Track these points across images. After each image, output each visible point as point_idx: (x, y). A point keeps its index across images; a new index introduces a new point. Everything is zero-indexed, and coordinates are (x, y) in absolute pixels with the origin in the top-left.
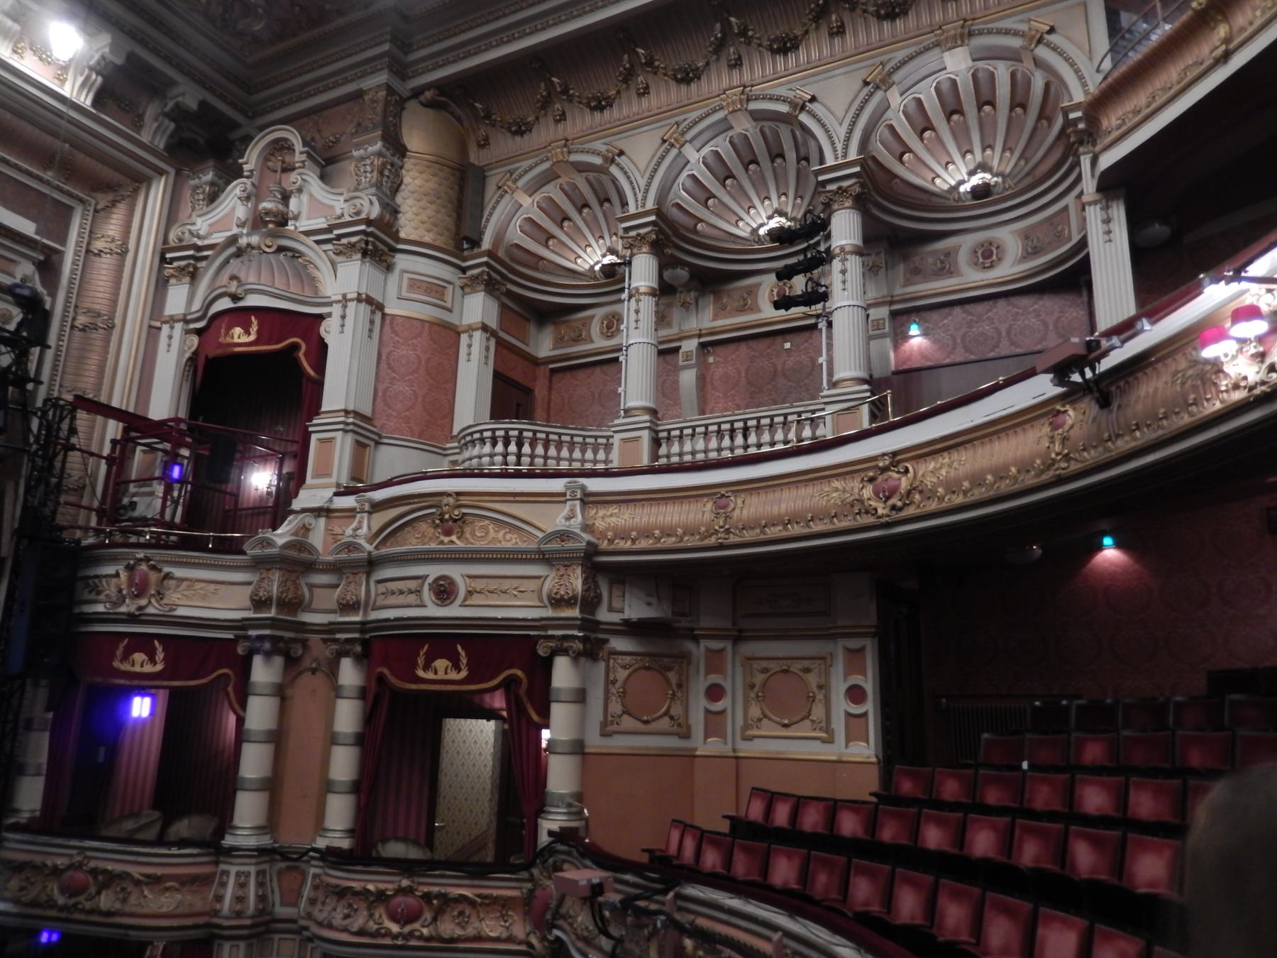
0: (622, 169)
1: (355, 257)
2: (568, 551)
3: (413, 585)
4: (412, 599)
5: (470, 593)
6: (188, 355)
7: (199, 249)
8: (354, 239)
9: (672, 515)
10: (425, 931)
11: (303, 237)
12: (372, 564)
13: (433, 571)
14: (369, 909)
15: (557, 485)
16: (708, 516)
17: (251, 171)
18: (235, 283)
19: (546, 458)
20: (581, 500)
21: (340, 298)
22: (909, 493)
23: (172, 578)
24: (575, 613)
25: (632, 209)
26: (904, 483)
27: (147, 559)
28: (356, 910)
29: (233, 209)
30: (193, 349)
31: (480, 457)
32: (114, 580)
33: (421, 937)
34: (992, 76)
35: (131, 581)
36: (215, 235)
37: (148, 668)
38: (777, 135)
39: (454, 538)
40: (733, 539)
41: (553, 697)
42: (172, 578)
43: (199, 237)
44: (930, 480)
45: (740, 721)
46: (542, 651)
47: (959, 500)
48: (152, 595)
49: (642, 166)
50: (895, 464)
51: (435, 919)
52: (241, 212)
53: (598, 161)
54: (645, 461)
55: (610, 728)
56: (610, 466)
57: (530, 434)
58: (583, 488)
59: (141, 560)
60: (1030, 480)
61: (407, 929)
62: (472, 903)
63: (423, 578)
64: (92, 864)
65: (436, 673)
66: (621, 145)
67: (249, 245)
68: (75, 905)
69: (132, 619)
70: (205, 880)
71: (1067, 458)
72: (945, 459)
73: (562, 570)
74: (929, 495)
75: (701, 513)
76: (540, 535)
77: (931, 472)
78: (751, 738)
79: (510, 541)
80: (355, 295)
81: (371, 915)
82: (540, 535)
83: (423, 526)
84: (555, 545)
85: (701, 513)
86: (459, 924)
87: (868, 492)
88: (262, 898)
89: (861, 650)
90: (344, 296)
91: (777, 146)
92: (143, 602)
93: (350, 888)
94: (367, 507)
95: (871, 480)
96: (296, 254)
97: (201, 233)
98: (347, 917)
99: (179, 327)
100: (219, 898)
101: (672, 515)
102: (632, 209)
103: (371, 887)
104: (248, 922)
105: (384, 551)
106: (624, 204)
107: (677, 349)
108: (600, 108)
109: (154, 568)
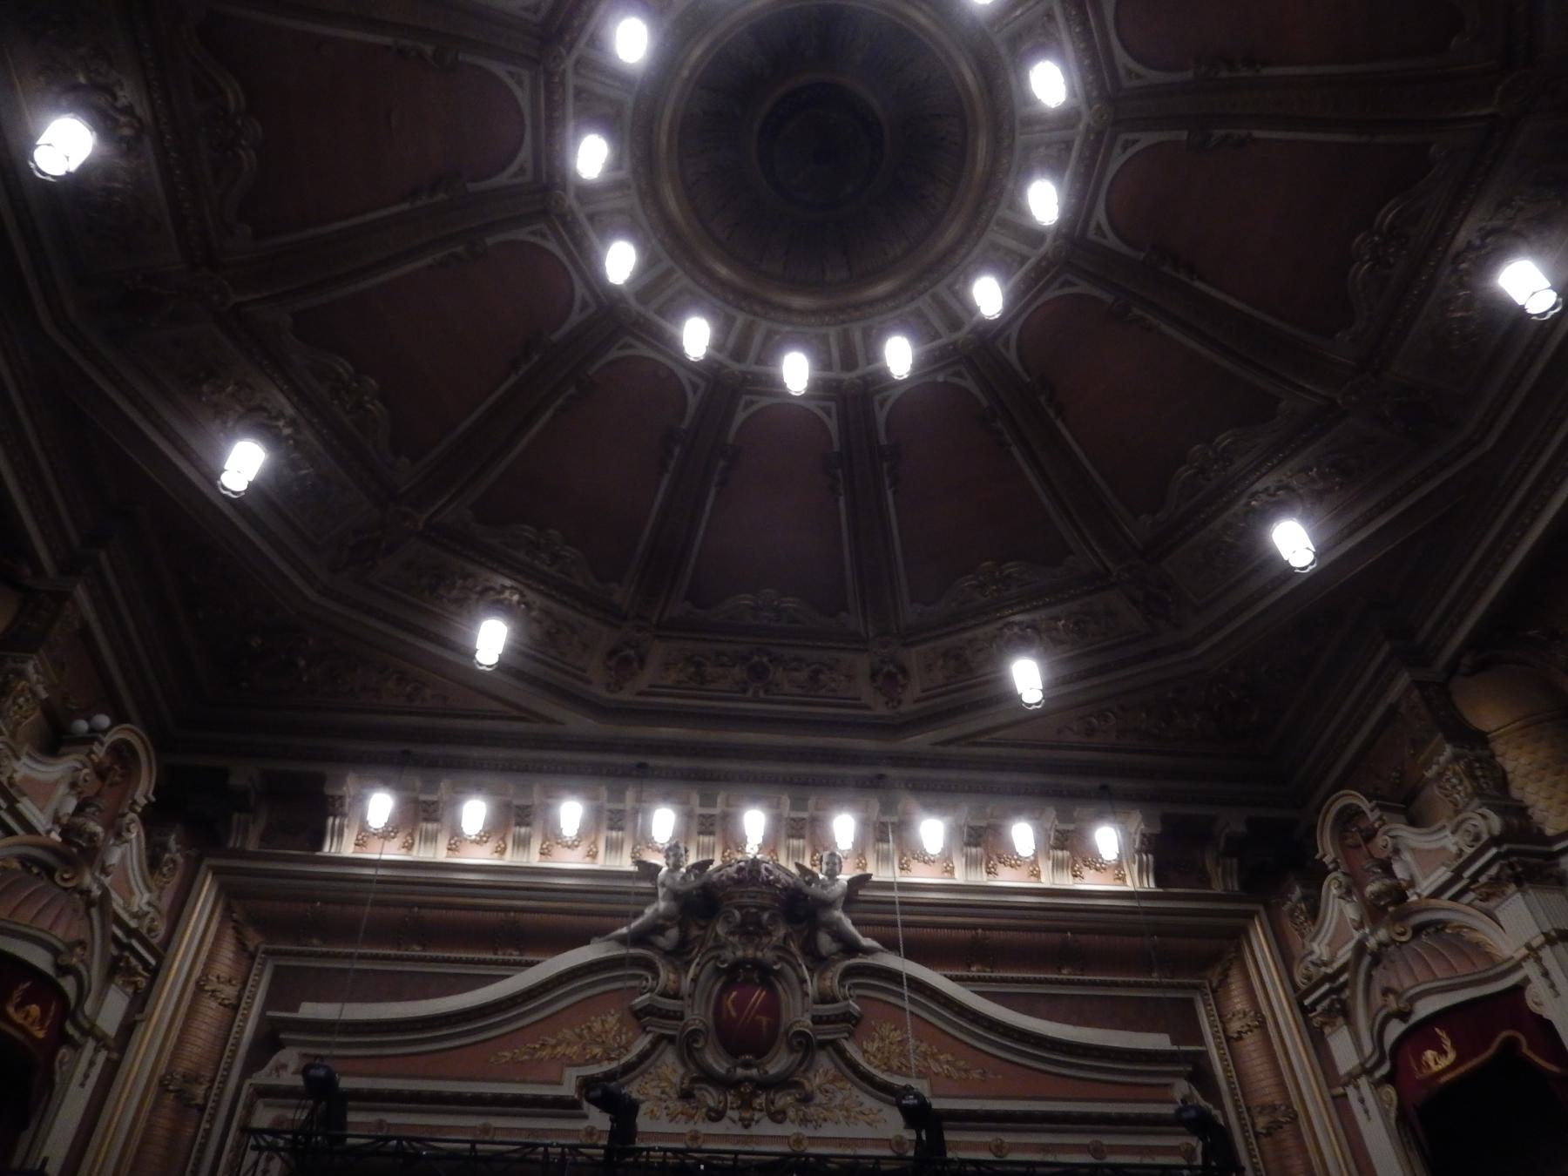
6: (1393, 1115)
7: (1332, 978)
8: (1493, 871)
36: (1340, 953)
43: (1325, 964)
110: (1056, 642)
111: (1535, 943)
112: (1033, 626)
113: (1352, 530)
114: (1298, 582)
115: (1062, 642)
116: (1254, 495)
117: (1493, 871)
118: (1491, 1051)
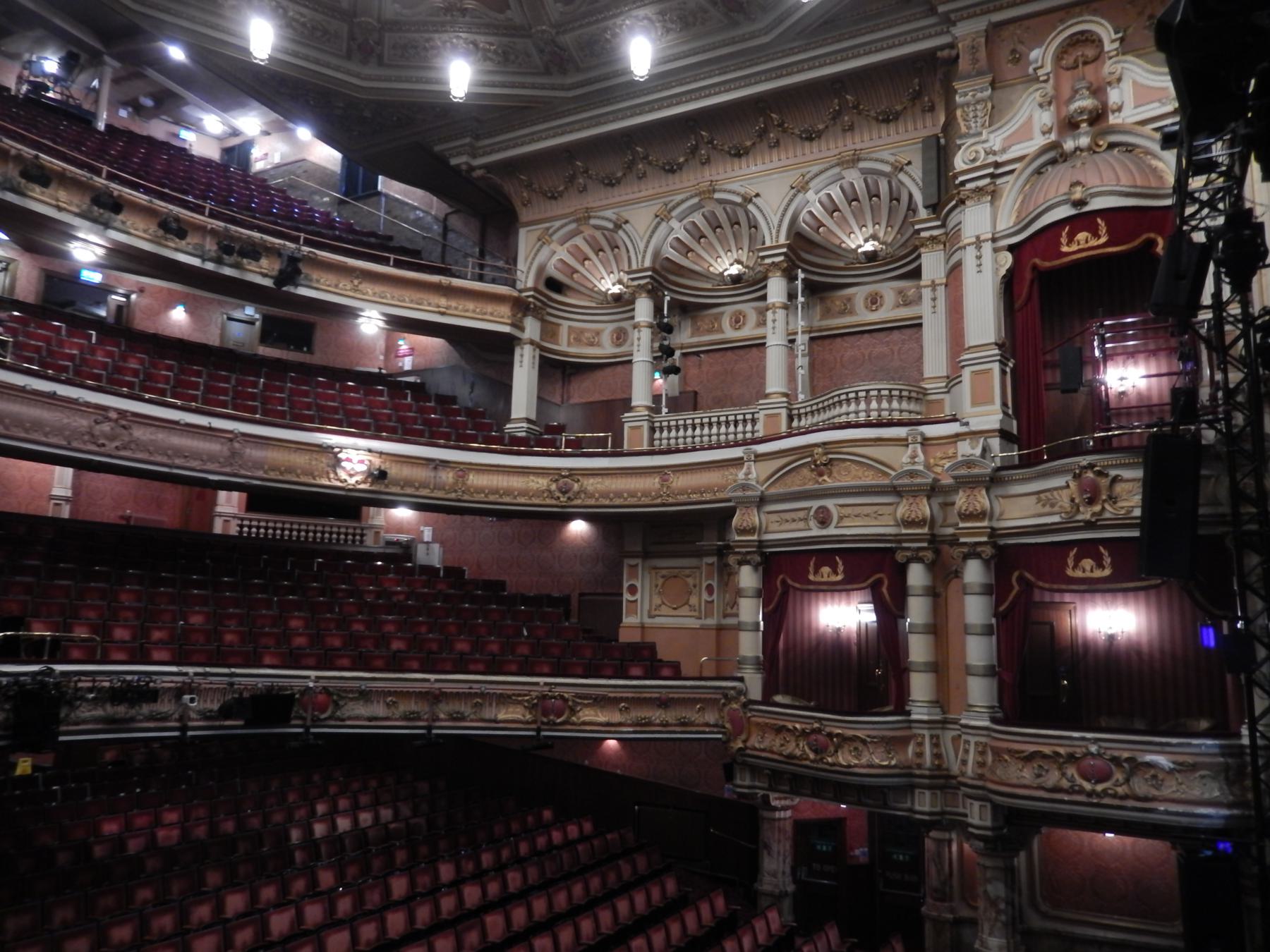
0: (758, 207)
1: (984, 199)
2: (972, 476)
3: (801, 514)
4: (801, 525)
5: (841, 518)
6: (1003, 272)
7: (997, 165)
8: (981, 183)
9: (516, 482)
10: (1120, 790)
11: (1139, 129)
12: (762, 501)
13: (815, 504)
14: (1060, 769)
15: (901, 432)
16: (657, 486)
17: (1048, 74)
18: (1079, 189)
19: (735, 434)
20: (922, 444)
21: (974, 240)
23: (1123, 480)
24: (926, 530)
27: (1091, 466)
28: (1047, 771)
29: (1031, 117)
30: (1008, 266)
31: (848, 414)
32: (1065, 491)
33: (1115, 796)
34: (577, 246)
35: (1082, 491)
36: (1014, 148)
37: (1098, 574)
38: (735, 213)
39: (825, 477)
41: (911, 592)
42: (1123, 480)
43: (995, 153)
45: (646, 607)
46: (900, 557)
48: (1104, 501)
51: (1127, 781)
52: (1046, 118)
54: (645, 447)
55: (654, 613)
56: (756, 435)
57: (886, 392)
58: (922, 434)
59: (1085, 467)
61: (1099, 788)
62: (864, 742)
63: (809, 509)
64: (828, 729)
65: (1084, 571)
67: (1077, 149)
68: (1104, 791)
69: (1089, 525)
70: (905, 741)
72: (599, 479)
73: (911, 500)
75: (653, 483)
76: (893, 473)
77: (591, 484)
78: (653, 617)
79: (869, 479)
80: (990, 236)
81: (1064, 775)
82: (893, 473)
83: (805, 471)
84: (906, 481)
85: (653, 483)
86: (1153, 786)
87: (554, 487)
88: (937, 756)
89: (637, 565)
90: (978, 238)
91: (735, 221)
92: (1097, 508)
93: (784, 726)
95: (556, 481)
96: (1129, 148)
97: (996, 148)
98: (782, 745)
99: (987, 248)
100: (920, 755)
101: (516, 482)
103: (1062, 751)
104: (927, 773)
105: (773, 491)
109: (1100, 474)
110: (486, 59)
111: (937, 282)
112: (475, 44)
113: (484, 85)
114: (806, 9)
115: (490, 59)
116: (458, 37)
117: (981, 183)
118: (1047, 264)
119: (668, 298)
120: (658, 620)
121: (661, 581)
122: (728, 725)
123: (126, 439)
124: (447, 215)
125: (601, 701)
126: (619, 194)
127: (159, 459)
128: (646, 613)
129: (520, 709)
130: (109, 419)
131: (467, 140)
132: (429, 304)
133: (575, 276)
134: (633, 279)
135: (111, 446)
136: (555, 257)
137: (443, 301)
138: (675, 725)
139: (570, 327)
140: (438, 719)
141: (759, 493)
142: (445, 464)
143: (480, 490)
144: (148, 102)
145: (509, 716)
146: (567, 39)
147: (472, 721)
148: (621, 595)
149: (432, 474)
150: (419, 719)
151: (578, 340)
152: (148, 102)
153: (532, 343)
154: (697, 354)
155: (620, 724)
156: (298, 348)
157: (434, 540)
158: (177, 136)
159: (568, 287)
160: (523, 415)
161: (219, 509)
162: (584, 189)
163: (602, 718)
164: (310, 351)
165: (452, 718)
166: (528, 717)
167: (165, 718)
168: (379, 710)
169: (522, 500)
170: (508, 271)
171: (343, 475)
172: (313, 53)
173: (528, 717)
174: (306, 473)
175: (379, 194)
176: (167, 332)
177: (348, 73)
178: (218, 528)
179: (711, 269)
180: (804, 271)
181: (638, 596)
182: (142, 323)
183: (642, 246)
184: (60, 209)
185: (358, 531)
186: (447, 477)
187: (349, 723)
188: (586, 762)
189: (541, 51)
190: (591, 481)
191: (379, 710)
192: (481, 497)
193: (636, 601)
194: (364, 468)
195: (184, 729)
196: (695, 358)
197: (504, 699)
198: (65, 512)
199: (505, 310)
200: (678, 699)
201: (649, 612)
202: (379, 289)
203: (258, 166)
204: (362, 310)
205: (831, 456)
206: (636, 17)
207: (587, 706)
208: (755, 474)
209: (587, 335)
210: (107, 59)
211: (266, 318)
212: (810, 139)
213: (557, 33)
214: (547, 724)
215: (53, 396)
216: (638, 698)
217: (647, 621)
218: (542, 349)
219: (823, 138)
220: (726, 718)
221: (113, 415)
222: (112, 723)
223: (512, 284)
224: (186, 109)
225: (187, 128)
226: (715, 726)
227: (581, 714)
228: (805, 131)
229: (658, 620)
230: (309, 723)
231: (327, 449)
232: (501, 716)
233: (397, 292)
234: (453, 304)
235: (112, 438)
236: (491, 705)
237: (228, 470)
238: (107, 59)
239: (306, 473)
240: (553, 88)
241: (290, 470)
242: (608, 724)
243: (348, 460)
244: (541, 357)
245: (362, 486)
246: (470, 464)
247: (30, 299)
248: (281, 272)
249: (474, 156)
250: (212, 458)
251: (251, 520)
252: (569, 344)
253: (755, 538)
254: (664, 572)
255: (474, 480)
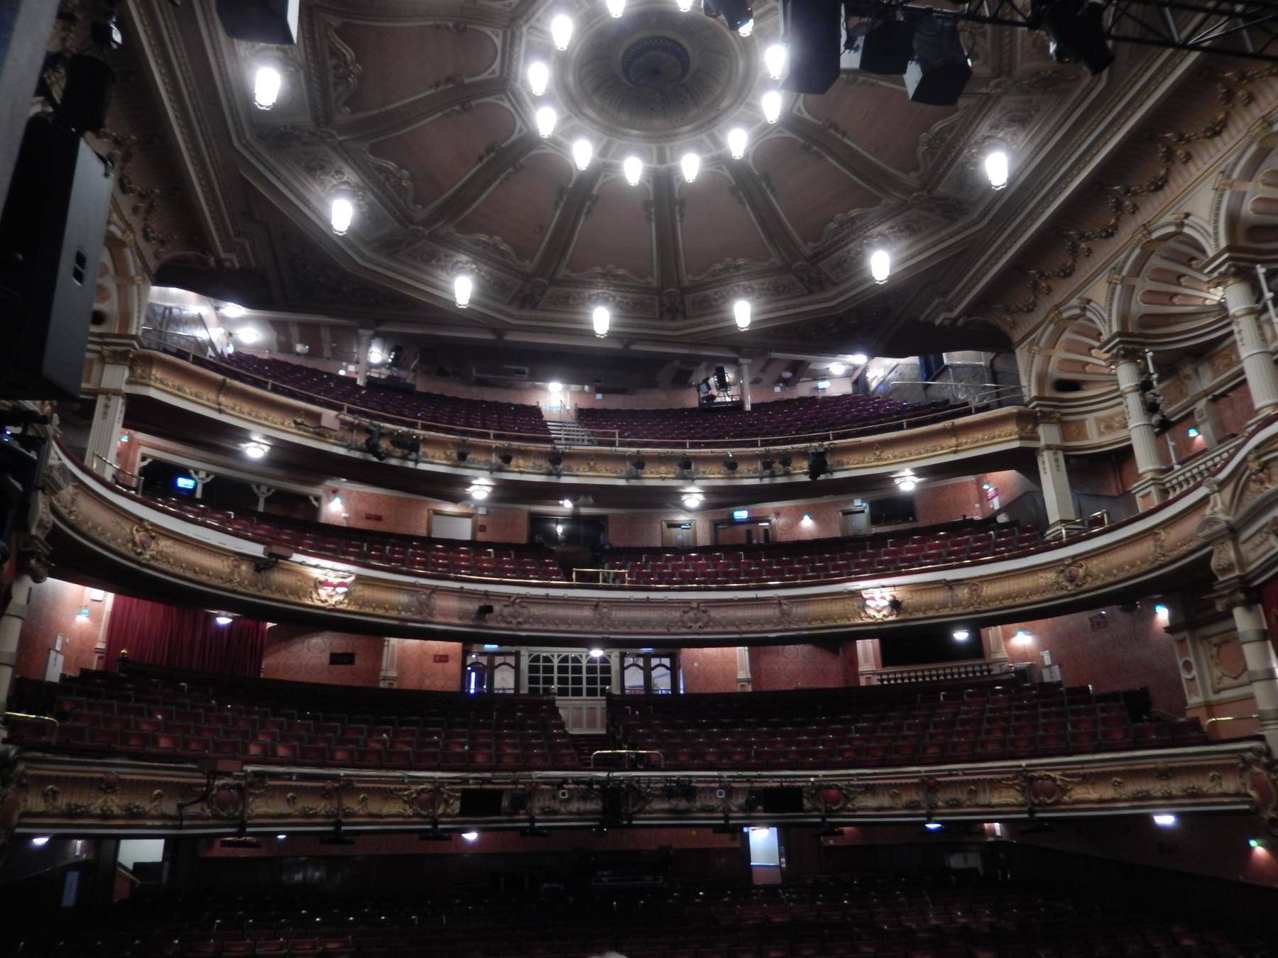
0: (1191, 227)
9: (1026, 583)
22: (1085, 577)
25: (1211, 253)
26: (1081, 571)
40: (983, 608)
44: (1095, 570)
45: (1208, 683)
47: (1111, 579)
49: (1206, 217)
50: (1074, 562)
53: (1172, 229)
60: (1146, 567)
66: (1186, 209)
71: (1164, 555)
72: (1102, 559)
74: (1097, 577)
75: (1146, 548)
77: (1095, 565)
85: (1147, 547)
94: (1216, 488)
101: (1026, 583)
102: (1211, 253)
106: (1203, 251)
107: (1191, 413)
108: (1110, 235)
119: (1150, 354)
120: (1226, 695)
121: (1215, 650)
122: (1253, 793)
123: (706, 619)
124: (992, 361)
125: (1088, 779)
126: (1077, 279)
127: (730, 629)
128: (1210, 691)
129: (1013, 792)
130: (692, 608)
131: (937, 301)
132: (943, 448)
133: (1087, 368)
134: (1107, 352)
135: (696, 627)
136: (1058, 361)
137: (953, 441)
138: (1182, 797)
139: (1099, 421)
140: (937, 807)
141: (1223, 525)
142: (959, 582)
143: (994, 598)
144: (788, 375)
145: (1002, 800)
146: (942, 190)
147: (968, 807)
148: (1179, 676)
149: (949, 594)
150: (921, 808)
151: (1109, 427)
152: (788, 375)
153: (1049, 447)
154: (1224, 395)
155: (1113, 800)
156: (905, 520)
157: (1054, 663)
158: (817, 388)
159: (1085, 382)
160: (1057, 518)
161: (861, 669)
162: (1049, 290)
163: (1094, 795)
164: (915, 520)
165: (949, 805)
166: (1021, 799)
167: (712, 810)
168: (885, 801)
169: (1035, 598)
170: (1013, 391)
171: (872, 612)
172: (782, 304)
173: (1021, 799)
174: (841, 617)
175: (947, 367)
176: (802, 538)
177: (818, 302)
178: (863, 682)
179: (1208, 302)
180: (1263, 262)
181: (1194, 673)
182: (783, 537)
183: (1106, 316)
184: (663, 479)
185: (984, 668)
186: (963, 593)
187: (859, 813)
188: (1241, 878)
189: (931, 210)
190: (1095, 562)
191: (885, 801)
192: (997, 604)
193: (1193, 679)
194: (886, 603)
195: (727, 818)
196: (1225, 400)
197: (994, 785)
198: (749, 689)
199: (1012, 428)
200: (1181, 768)
201: (1213, 687)
202: (897, 452)
203: (874, 385)
204: (681, 487)
205: (1264, 459)
206: (976, 143)
207: (1077, 784)
208: (1219, 508)
209: (1117, 419)
210: (741, 360)
211: (873, 505)
212: (1218, 133)
213: (929, 192)
214: (1039, 805)
215: (648, 600)
216: (1130, 771)
217: (1214, 698)
218: (1065, 449)
219: (1230, 124)
220: (1249, 783)
221: (695, 605)
222: (675, 812)
223: (1018, 401)
224: (811, 367)
225: (824, 379)
226: (1237, 794)
227: (1072, 793)
228: (1208, 129)
229: (1226, 695)
230: (823, 813)
231: (856, 594)
232: (995, 801)
233: (913, 449)
234: (963, 440)
235: (696, 621)
236: (985, 791)
237: (781, 627)
238: (741, 360)
239: (841, 617)
240: (965, 228)
241: (828, 617)
242: (1101, 801)
243: (873, 599)
244: (1067, 458)
245: (890, 618)
246: (982, 577)
247: (708, 543)
248: (811, 467)
249: (951, 310)
250: (768, 620)
251: (888, 674)
252: (1101, 434)
253: (1237, 573)
254: (1215, 640)
255: (989, 590)
